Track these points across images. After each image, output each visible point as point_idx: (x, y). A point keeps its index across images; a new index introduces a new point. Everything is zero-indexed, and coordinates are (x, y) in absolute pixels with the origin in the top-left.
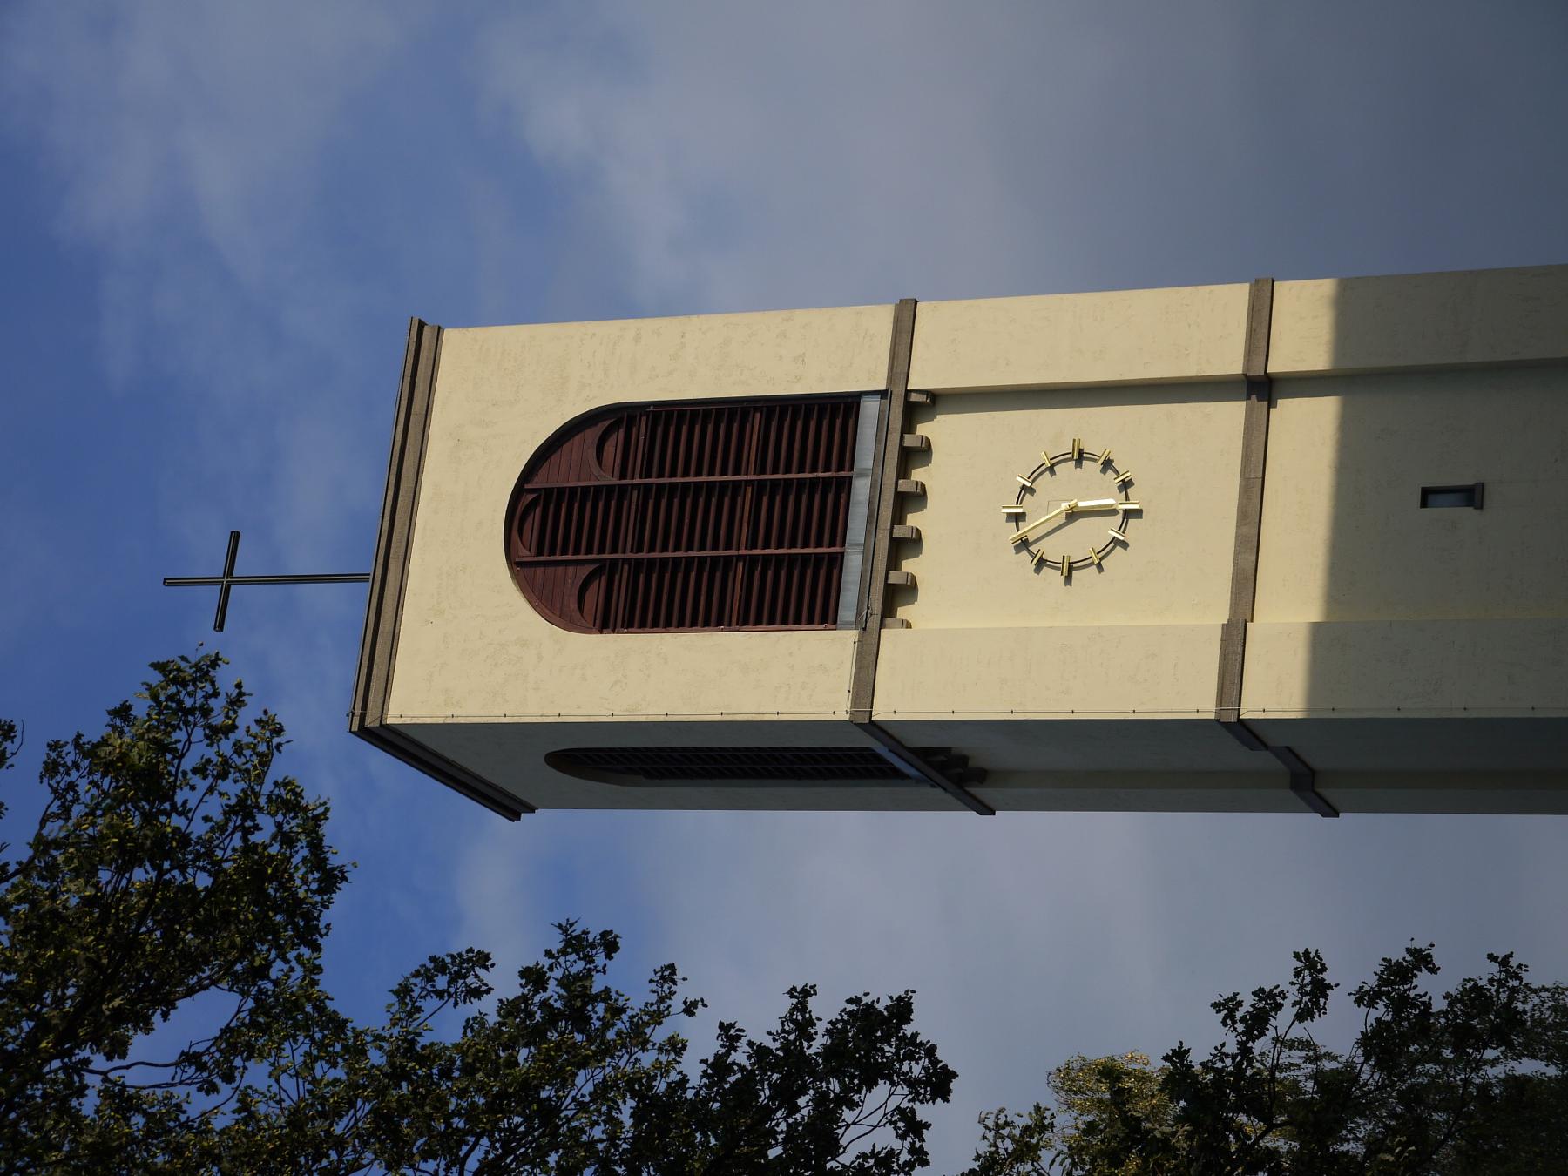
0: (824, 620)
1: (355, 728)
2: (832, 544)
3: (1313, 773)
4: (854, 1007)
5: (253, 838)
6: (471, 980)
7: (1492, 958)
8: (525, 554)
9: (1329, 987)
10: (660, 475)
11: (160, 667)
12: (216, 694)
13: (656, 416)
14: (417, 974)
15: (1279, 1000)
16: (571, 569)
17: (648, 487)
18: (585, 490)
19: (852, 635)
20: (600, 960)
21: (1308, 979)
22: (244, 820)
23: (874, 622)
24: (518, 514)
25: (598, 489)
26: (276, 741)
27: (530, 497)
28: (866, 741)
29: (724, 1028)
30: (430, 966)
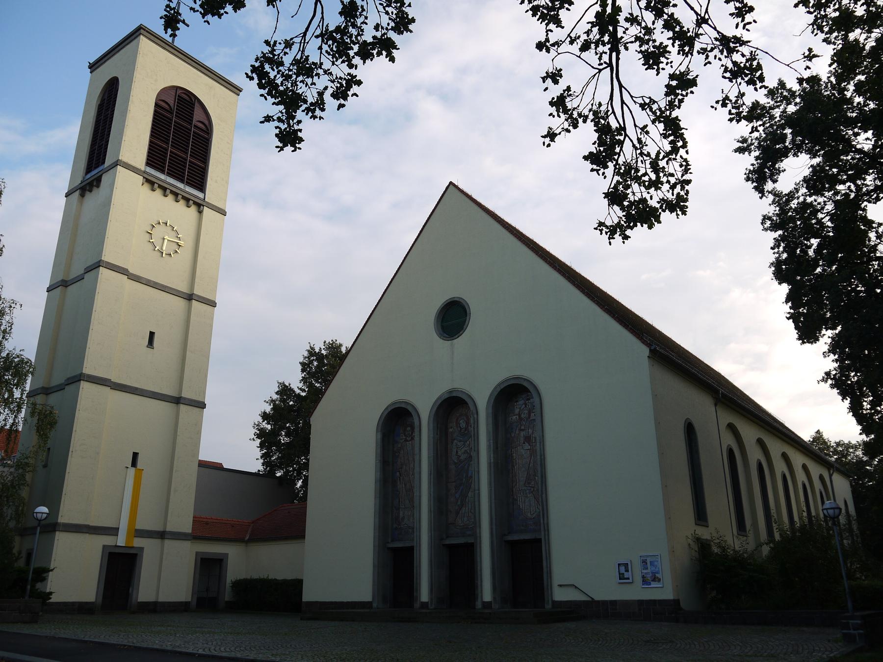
1: (142, 26)
2: (167, 172)
3: (66, 287)
16: (173, 102)
24: (190, 95)
27: (193, 100)
28: (108, 162)
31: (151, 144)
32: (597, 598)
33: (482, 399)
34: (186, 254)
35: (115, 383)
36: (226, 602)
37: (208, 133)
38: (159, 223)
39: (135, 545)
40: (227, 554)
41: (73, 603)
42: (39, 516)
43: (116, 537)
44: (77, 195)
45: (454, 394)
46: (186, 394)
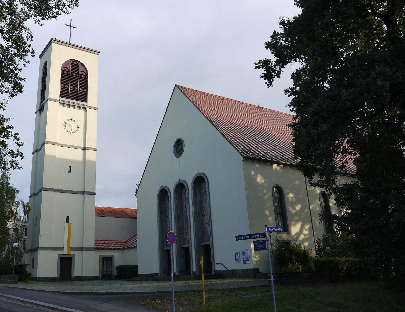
4: (22, 86)
5: (54, 9)
6: (29, 39)
9: (19, 146)
10: (79, 78)
12: (73, 6)
13: (86, 79)
14: (30, 32)
15: (18, 140)
16: (69, 67)
17: (78, 77)
19: (59, 99)
21: (21, 144)
22: (56, 8)
23: (60, 102)
26: (66, 13)
27: (78, 63)
30: (31, 34)
31: (62, 87)
32: (229, 269)
33: (190, 183)
34: (81, 130)
35: (56, 189)
36: (115, 275)
39: (71, 254)
40: (114, 255)
41: (48, 277)
43: (63, 251)
44: (38, 114)
45: (180, 182)
46: (86, 190)
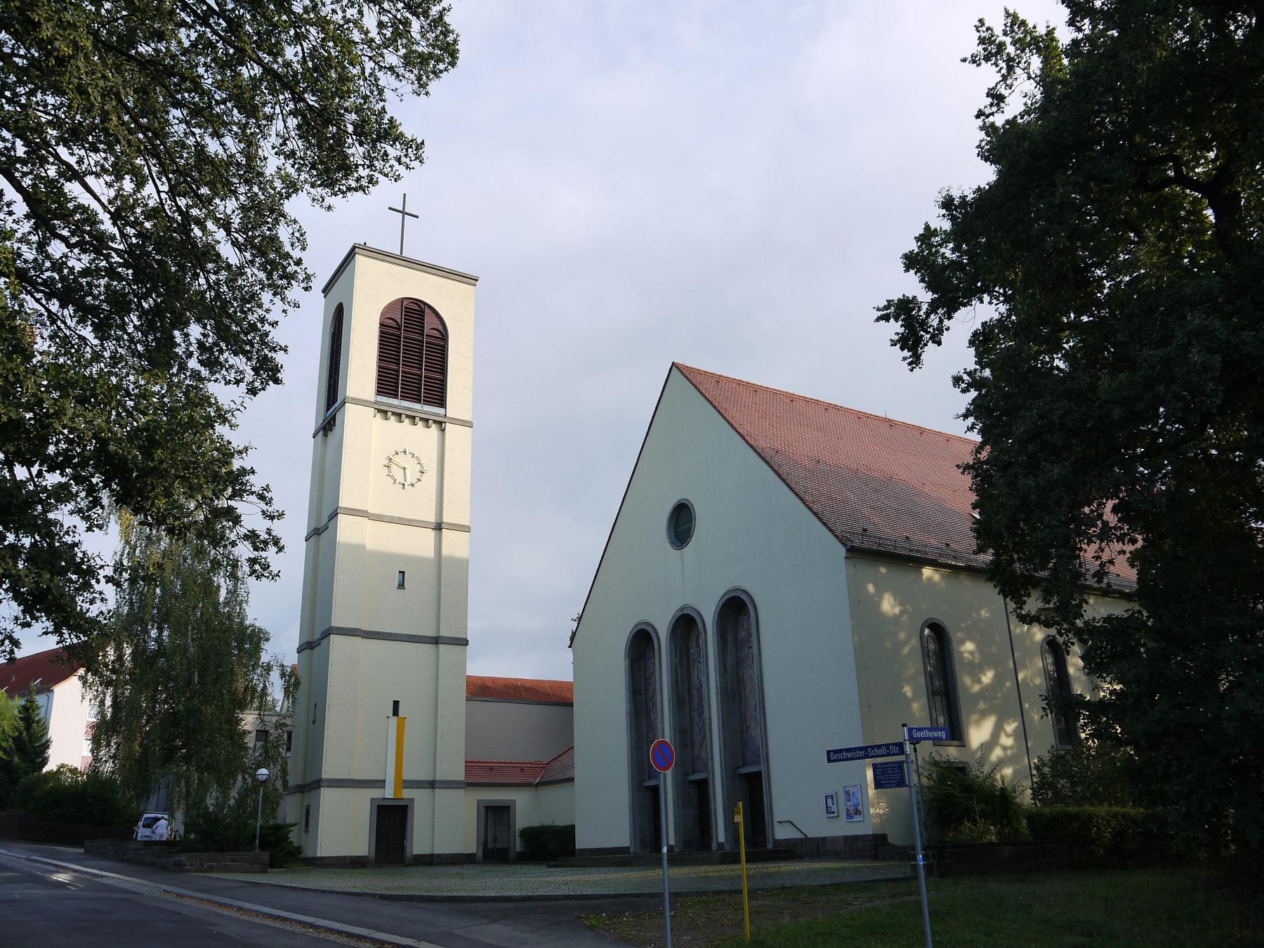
0: (378, 391)
5: (361, 167)
6: (297, 244)
7: (279, 572)
8: (405, 303)
11: (423, 143)
13: (444, 347)
18: (423, 323)
20: (303, 285)
23: (376, 406)
25: (423, 327)
28: (339, 400)
29: (277, 323)
32: (809, 836)
33: (709, 614)
34: (431, 478)
35: (366, 632)
36: (517, 853)
37: (444, 340)
38: (405, 452)
41: (345, 858)
42: (260, 777)
46: (445, 633)
